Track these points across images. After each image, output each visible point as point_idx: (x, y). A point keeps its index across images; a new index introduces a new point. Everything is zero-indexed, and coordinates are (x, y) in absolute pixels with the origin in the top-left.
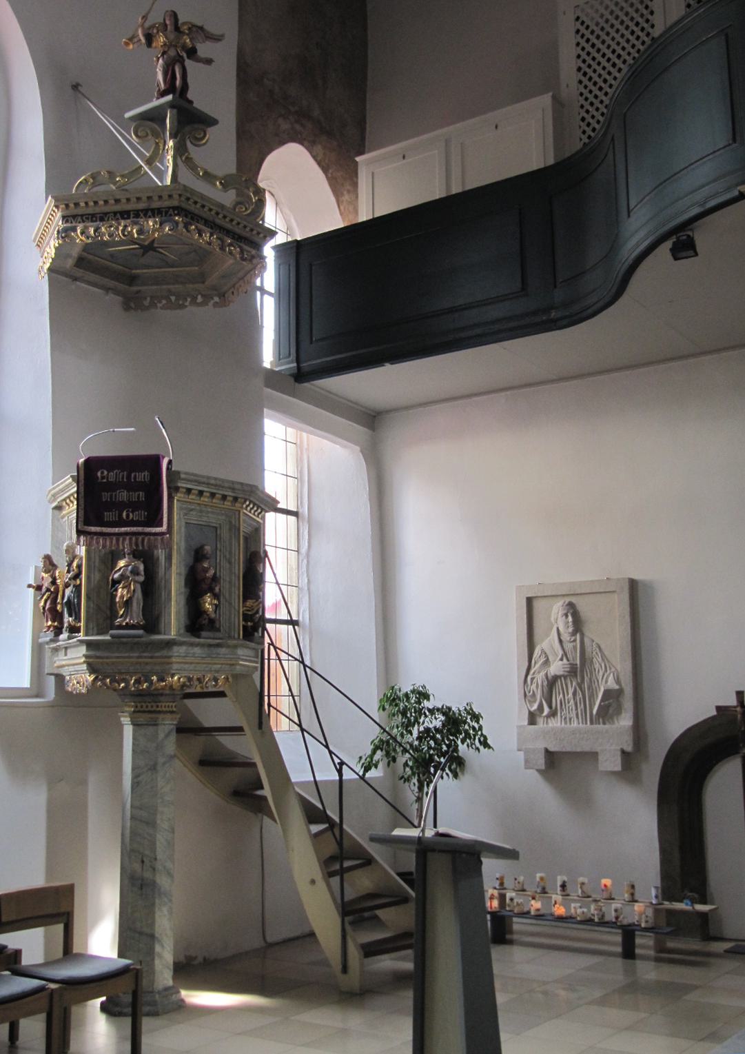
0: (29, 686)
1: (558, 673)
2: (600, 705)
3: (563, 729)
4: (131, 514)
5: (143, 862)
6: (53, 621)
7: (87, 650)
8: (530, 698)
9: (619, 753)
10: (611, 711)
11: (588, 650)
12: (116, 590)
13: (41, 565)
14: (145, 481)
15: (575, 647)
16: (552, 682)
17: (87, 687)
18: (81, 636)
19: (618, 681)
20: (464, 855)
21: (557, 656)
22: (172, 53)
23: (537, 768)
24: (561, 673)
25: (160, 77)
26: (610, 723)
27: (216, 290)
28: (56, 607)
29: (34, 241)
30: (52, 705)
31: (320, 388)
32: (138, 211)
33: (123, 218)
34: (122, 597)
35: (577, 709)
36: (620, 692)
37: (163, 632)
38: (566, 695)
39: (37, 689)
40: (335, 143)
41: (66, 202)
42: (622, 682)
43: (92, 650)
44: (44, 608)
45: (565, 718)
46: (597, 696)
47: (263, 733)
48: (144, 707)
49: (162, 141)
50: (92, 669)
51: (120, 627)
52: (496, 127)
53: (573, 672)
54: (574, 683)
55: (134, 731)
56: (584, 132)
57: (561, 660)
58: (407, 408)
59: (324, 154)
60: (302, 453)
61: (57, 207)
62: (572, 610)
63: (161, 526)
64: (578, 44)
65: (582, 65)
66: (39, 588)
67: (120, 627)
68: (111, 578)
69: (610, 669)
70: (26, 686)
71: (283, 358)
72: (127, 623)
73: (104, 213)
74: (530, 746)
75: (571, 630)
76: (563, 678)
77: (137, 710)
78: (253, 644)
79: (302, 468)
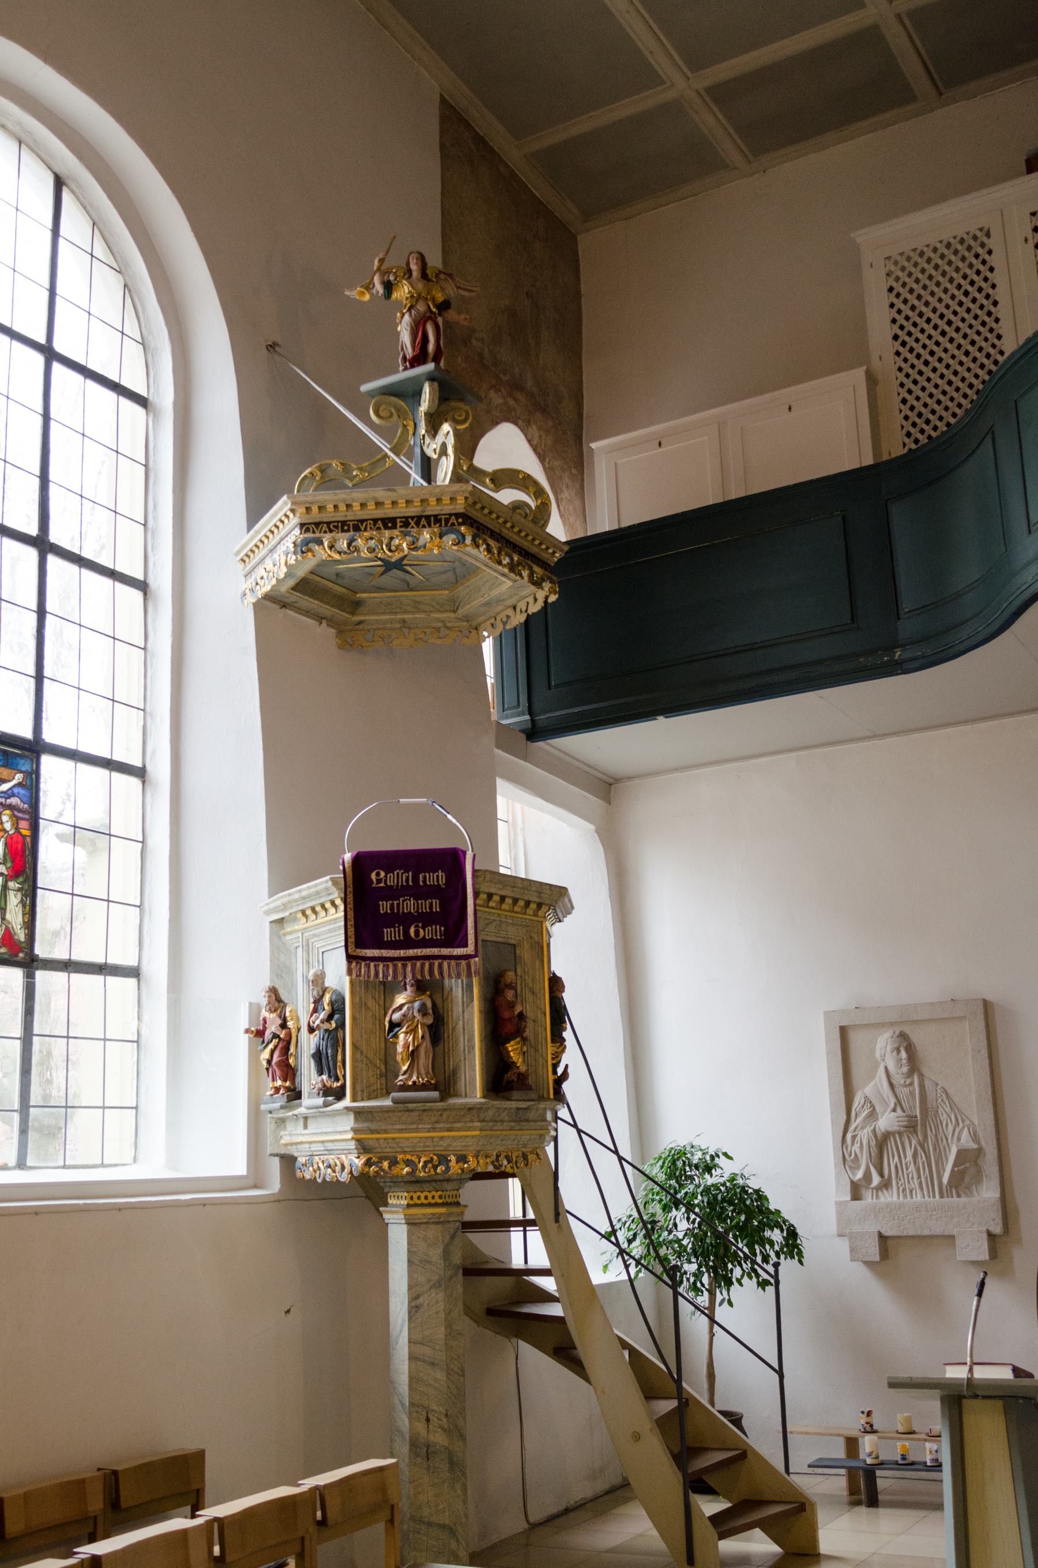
0: (245, 1173)
1: (890, 1129)
2: (952, 1171)
3: (901, 1206)
4: (421, 931)
5: (428, 1420)
6: (285, 1080)
7: (356, 1120)
8: (851, 1164)
9: (985, 1236)
10: (967, 1179)
11: (931, 1095)
12: (396, 1036)
13: (264, 1002)
14: (439, 885)
15: (912, 1094)
16: (882, 1142)
17: (351, 1172)
18: (347, 1102)
19: (975, 1137)
20: (1021, 1401)
21: (888, 1105)
22: (421, 307)
23: (867, 1259)
24: (896, 1128)
25: (406, 338)
26: (967, 1196)
27: (468, 621)
28: (287, 1059)
29: (237, 553)
30: (276, 1200)
31: (558, 750)
32: (407, 518)
33: (386, 527)
34: (406, 1046)
35: (919, 1177)
36: (980, 1151)
37: (463, 1094)
38: (904, 1156)
39: (255, 1177)
40: (550, 423)
41: (308, 505)
42: (982, 1139)
43: (364, 1121)
44: (269, 1062)
45: (904, 1190)
46: (947, 1159)
47: (559, 1227)
48: (422, 1197)
49: (412, 423)
50: (363, 1147)
51: (404, 1088)
52: (790, 409)
53: (911, 1126)
54: (914, 1142)
55: (410, 1234)
56: (906, 418)
57: (894, 1110)
58: (657, 773)
59: (540, 437)
60: (515, 835)
61: (292, 511)
62: (906, 1044)
63: (466, 945)
64: (892, 306)
65: (899, 332)
66: (260, 1033)
67: (404, 1088)
68: (387, 1019)
69: (963, 1122)
70: (240, 1174)
71: (509, 708)
72: (414, 1082)
73: (358, 521)
74: (857, 1229)
75: (905, 1069)
76: (897, 1136)
77: (411, 1202)
78: (513, 1103)
79: (515, 855)
